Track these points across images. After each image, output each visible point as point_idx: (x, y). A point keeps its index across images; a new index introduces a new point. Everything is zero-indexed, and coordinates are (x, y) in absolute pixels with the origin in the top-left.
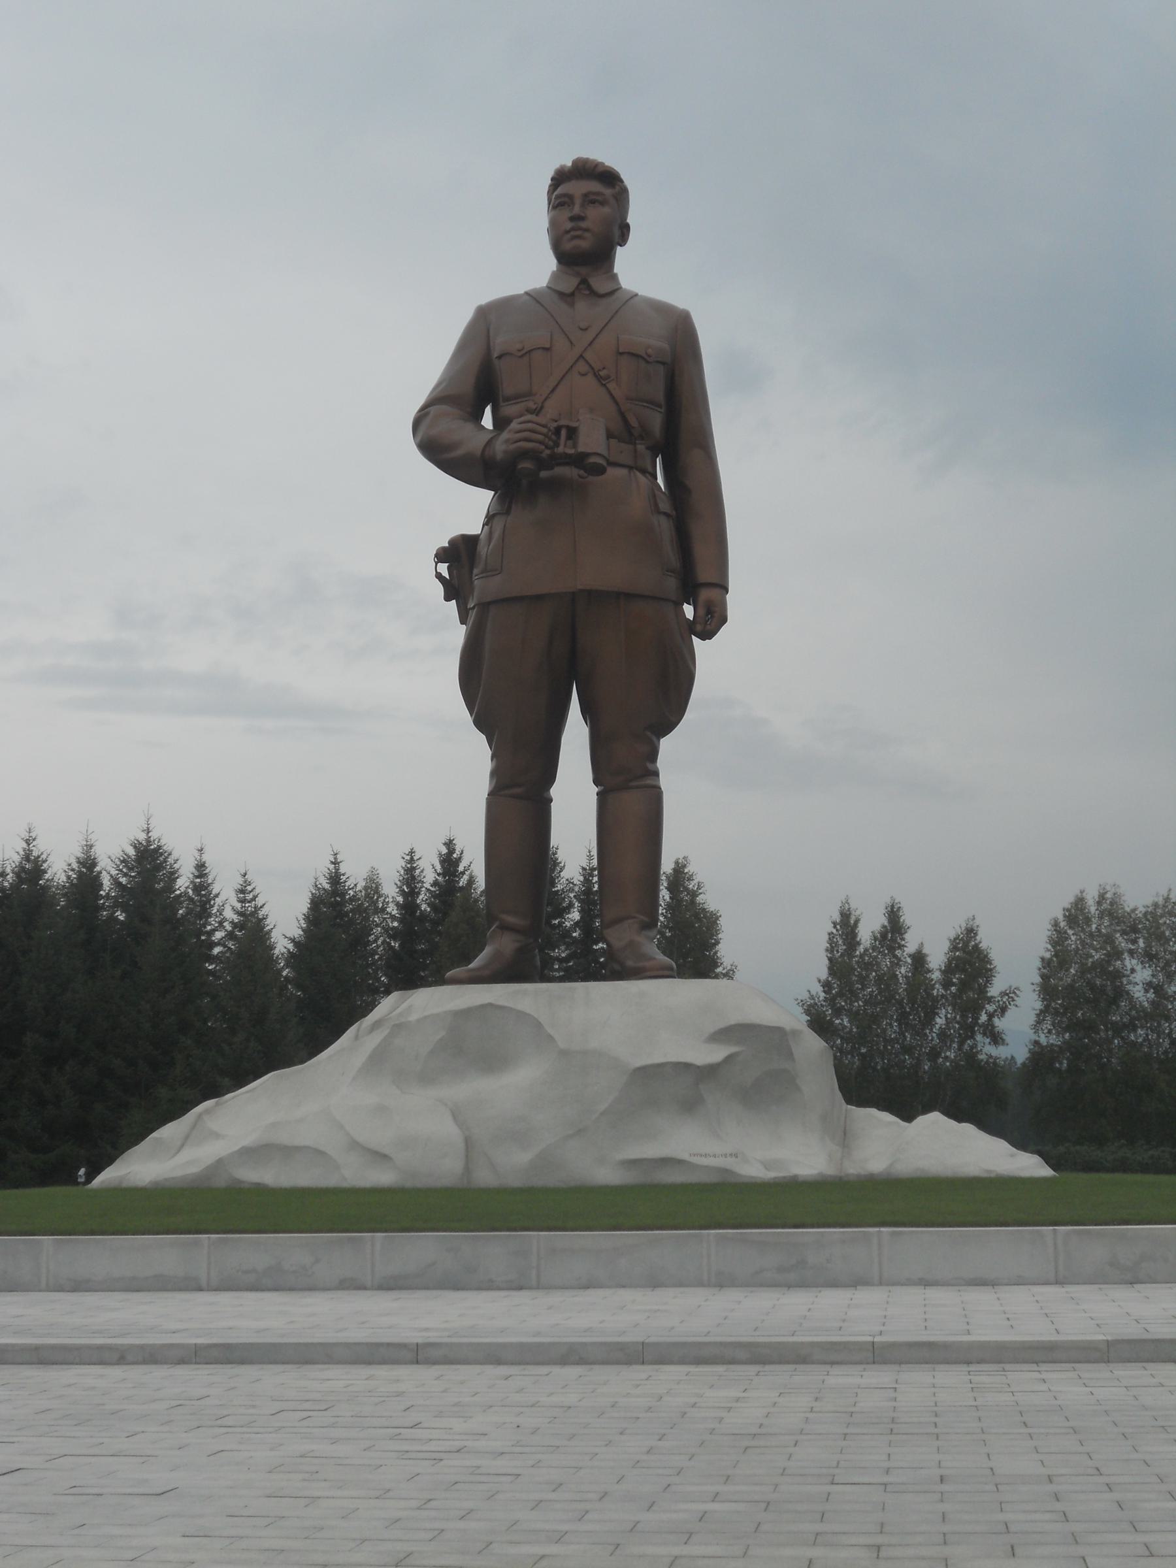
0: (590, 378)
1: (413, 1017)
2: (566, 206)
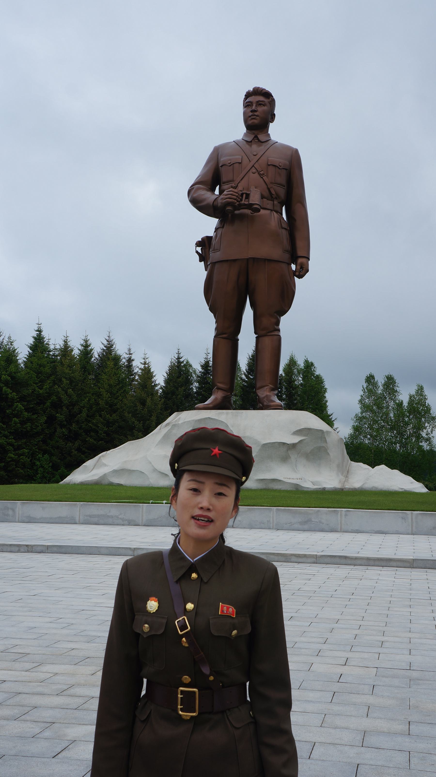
0: (256, 174)
1: (180, 422)
2: (250, 106)
